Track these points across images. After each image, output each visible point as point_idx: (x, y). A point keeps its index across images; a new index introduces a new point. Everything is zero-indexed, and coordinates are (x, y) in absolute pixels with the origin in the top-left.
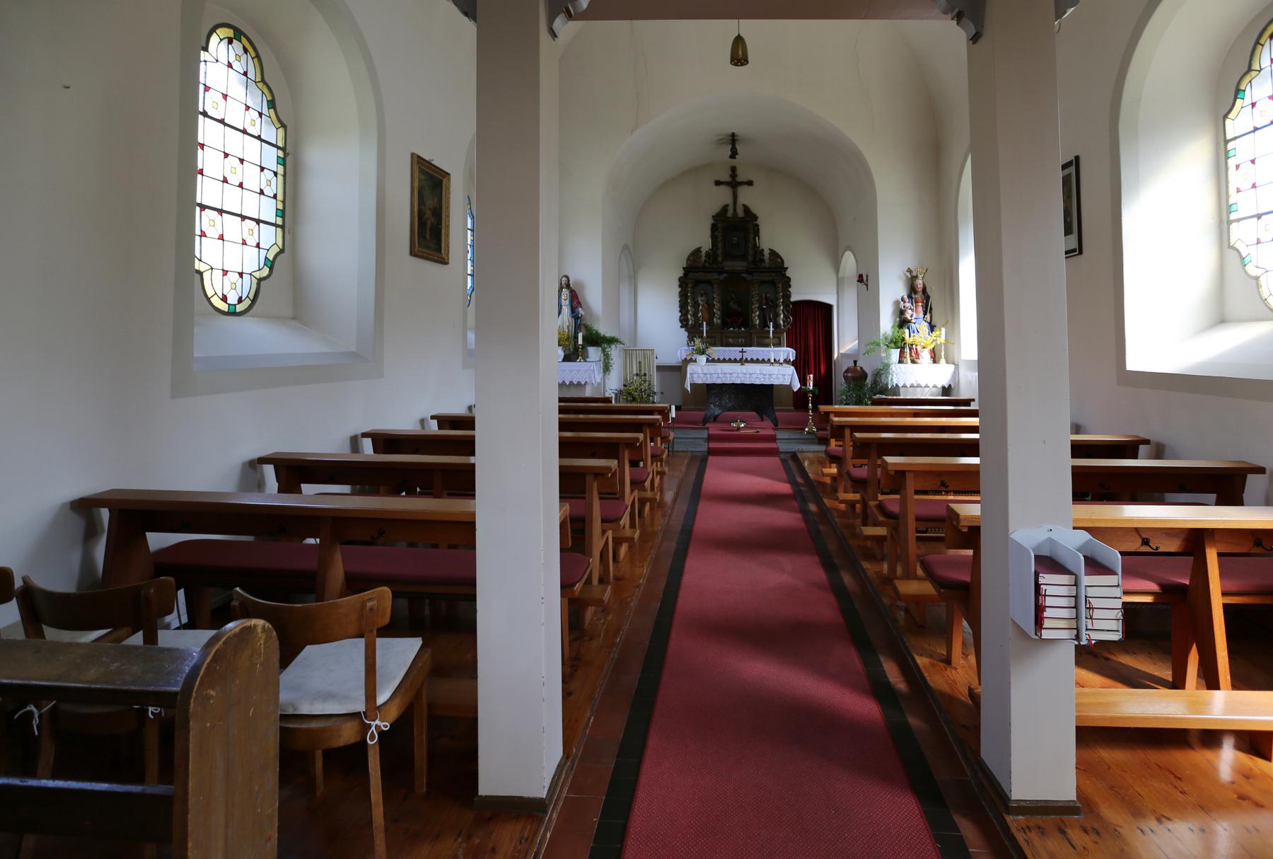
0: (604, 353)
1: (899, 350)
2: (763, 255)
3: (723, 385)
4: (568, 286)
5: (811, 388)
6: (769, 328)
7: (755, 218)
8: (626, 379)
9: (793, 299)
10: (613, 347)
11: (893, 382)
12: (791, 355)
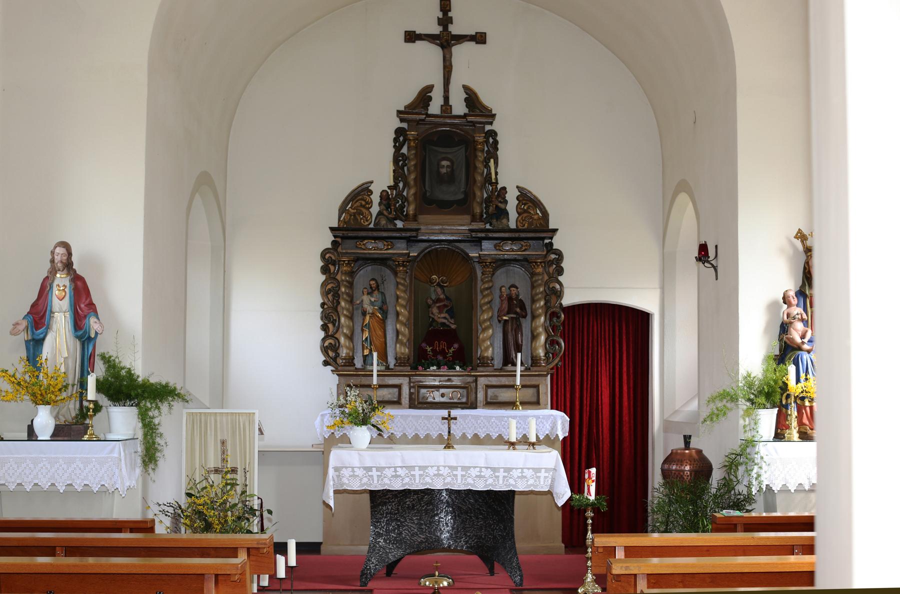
0: (143, 420)
1: (776, 410)
2: (506, 202)
3: (406, 493)
4: (68, 265)
5: (592, 497)
6: (514, 365)
7: (490, 116)
8: (191, 480)
9: (568, 300)
10: (164, 407)
11: (760, 483)
12: (559, 427)
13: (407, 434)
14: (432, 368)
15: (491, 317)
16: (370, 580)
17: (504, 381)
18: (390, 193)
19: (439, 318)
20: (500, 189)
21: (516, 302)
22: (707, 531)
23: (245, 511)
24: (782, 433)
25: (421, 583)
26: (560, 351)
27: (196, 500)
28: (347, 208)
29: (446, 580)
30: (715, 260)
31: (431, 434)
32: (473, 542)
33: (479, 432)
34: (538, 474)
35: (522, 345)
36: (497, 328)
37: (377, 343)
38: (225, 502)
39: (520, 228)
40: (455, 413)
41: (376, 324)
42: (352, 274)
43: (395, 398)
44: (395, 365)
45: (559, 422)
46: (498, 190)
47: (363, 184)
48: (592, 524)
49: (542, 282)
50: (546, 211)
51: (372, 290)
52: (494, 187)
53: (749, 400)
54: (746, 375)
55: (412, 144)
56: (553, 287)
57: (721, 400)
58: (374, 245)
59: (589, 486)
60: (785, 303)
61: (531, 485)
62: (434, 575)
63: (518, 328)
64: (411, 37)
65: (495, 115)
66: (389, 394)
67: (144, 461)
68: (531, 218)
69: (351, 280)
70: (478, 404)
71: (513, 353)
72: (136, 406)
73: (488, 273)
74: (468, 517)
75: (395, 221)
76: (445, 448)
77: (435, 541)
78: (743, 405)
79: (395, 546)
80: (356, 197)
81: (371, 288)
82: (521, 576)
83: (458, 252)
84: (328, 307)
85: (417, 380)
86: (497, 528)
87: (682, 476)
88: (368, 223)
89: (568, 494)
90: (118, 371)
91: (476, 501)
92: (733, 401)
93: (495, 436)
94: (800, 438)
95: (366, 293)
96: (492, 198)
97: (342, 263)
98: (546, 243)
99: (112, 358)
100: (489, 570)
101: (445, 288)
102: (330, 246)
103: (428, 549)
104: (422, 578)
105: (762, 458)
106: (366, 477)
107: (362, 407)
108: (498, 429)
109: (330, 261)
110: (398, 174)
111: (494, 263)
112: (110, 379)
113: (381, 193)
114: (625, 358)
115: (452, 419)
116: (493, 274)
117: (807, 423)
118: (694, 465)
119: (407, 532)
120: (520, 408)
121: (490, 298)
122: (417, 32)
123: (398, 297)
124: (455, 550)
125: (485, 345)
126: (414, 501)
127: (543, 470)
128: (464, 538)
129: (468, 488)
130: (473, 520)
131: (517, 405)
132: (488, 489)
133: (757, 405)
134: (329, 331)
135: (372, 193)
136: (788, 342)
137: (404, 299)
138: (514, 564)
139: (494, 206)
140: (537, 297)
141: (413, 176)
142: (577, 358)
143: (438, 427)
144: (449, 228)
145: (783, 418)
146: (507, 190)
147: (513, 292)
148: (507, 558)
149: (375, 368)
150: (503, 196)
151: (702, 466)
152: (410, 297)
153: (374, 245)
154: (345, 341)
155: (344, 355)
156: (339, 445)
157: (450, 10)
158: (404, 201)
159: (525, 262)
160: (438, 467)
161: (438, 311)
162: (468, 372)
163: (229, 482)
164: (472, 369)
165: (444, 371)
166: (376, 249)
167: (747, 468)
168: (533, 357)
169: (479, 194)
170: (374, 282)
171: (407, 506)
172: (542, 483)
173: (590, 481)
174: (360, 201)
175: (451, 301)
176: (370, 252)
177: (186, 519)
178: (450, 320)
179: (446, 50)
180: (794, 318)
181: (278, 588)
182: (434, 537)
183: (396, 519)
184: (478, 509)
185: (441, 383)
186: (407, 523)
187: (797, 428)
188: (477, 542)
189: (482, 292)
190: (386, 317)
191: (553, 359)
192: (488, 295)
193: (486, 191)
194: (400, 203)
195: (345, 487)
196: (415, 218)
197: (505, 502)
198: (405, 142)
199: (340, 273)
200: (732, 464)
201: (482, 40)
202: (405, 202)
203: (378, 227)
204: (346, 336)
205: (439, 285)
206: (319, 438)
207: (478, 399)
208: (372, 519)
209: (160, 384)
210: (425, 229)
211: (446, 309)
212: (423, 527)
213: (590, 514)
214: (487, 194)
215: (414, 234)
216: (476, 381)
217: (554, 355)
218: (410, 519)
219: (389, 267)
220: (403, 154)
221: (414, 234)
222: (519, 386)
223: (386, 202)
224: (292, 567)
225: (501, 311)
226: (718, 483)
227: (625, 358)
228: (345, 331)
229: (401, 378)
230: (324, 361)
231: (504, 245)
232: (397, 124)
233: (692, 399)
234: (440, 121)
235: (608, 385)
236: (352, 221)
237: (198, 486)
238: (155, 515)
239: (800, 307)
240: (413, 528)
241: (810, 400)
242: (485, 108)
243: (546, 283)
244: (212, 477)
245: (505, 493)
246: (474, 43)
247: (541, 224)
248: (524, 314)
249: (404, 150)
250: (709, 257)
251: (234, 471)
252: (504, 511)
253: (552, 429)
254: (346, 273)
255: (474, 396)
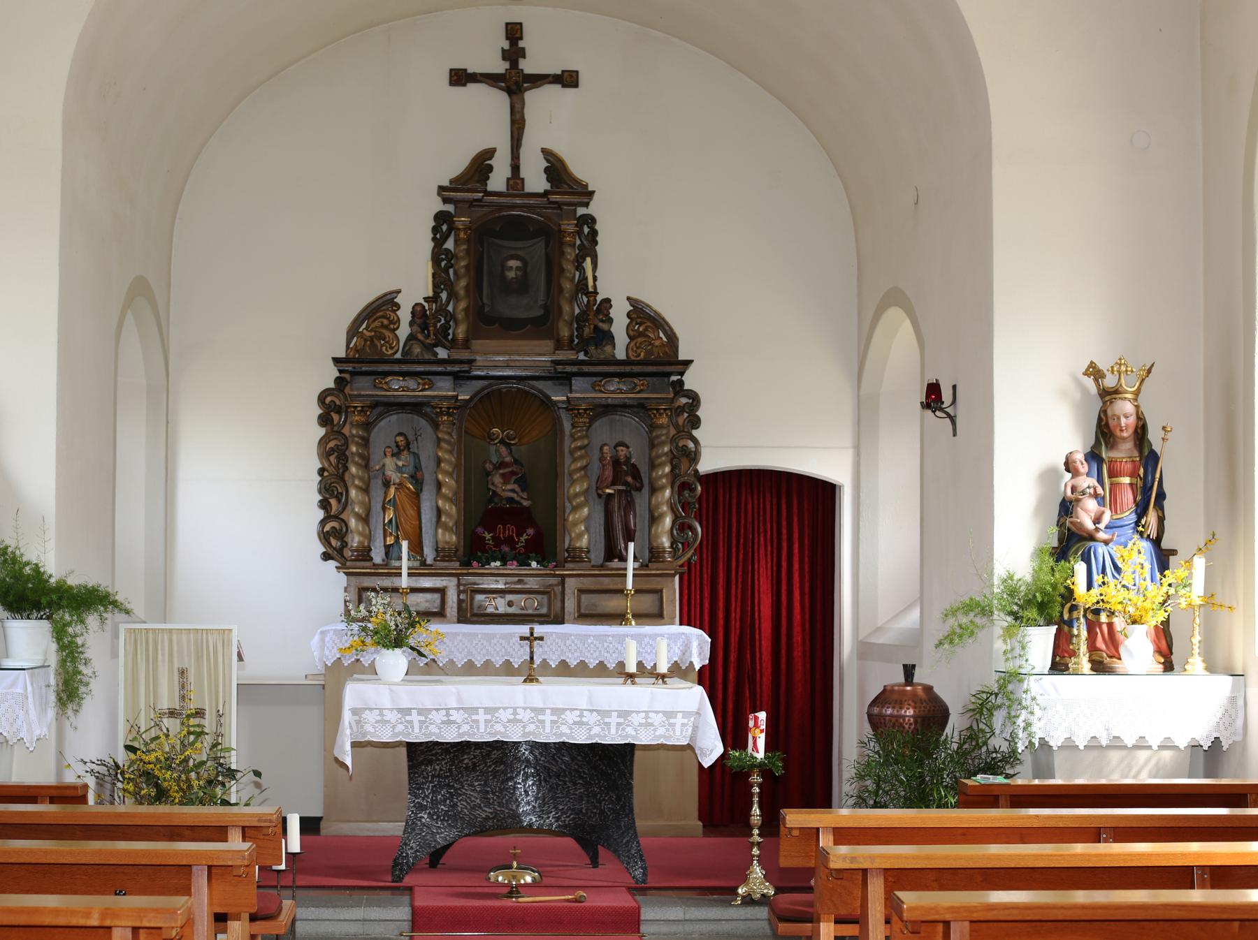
5: (760, 755)
6: (623, 559)
7: (587, 195)
8: (133, 727)
9: (708, 463)
10: (92, 620)
13: (455, 660)
14: (493, 564)
15: (587, 491)
16: (406, 873)
17: (607, 583)
18: (427, 308)
19: (504, 490)
20: (601, 302)
21: (627, 467)
22: (946, 806)
23: (220, 772)
24: (1062, 662)
25: (490, 878)
26: (695, 540)
27: (144, 757)
28: (361, 330)
29: (530, 874)
30: (953, 406)
31: (493, 660)
32: (568, 819)
33: (568, 657)
34: (672, 721)
35: (635, 531)
36: (596, 506)
37: (408, 528)
38: (186, 760)
39: (633, 358)
40: (539, 629)
41: (405, 499)
42: (368, 426)
43: (436, 608)
44: (435, 560)
45: (695, 644)
46: (598, 302)
47: (385, 295)
48: (760, 795)
49: (667, 438)
50: (674, 334)
51: (399, 449)
52: (591, 299)
53: (1011, 613)
54: (1005, 578)
55: (462, 235)
56: (684, 446)
57: (966, 614)
58: (402, 383)
59: (755, 739)
60: (1068, 470)
61: (661, 736)
62: (510, 867)
63: (629, 506)
64: (460, 78)
65: (593, 192)
66: (427, 601)
67: (60, 699)
68: (650, 344)
69: (366, 435)
70: (566, 617)
71: (622, 541)
72: (48, 618)
73: (581, 425)
74: (560, 783)
75: (435, 349)
76: (525, 681)
77: (509, 816)
78: (1002, 621)
79: (446, 824)
80: (374, 314)
81: (398, 446)
82: (644, 869)
83: (534, 394)
84: (330, 475)
85: (469, 581)
86: (606, 798)
87: (901, 724)
88: (392, 352)
89: (719, 749)
90: (20, 568)
91: (573, 759)
92: (985, 615)
93: (592, 663)
94: (1092, 669)
95: (390, 454)
96: (588, 315)
97: (353, 409)
98: (673, 381)
99: (10, 550)
100: (591, 859)
101: (512, 447)
102: (332, 385)
103: (497, 829)
104: (491, 871)
105: (1034, 699)
106: (401, 723)
107: (395, 621)
108: (597, 653)
109: (333, 407)
110: (440, 280)
111: (591, 410)
112: (7, 579)
113: (413, 308)
114: (796, 551)
115: (536, 639)
116: (590, 426)
117: (1103, 647)
118: (920, 707)
119: (464, 803)
120: (633, 623)
121: (584, 462)
122: (470, 71)
123: (439, 461)
124: (540, 831)
125: (577, 531)
126: (475, 757)
127: (680, 715)
128: (554, 813)
129: (561, 741)
130: (569, 787)
131: (628, 619)
132: (594, 741)
133: (1025, 620)
134: (331, 510)
135: (399, 307)
136: (1073, 529)
137: (449, 462)
138: (633, 852)
139: (592, 327)
140: (660, 460)
141: (463, 283)
142: (721, 550)
143: (503, 650)
144: (521, 359)
145: (1064, 640)
146: (612, 303)
147: (621, 453)
148: (622, 842)
149: (405, 563)
150: (605, 312)
151: (934, 710)
152: (458, 459)
153: (402, 383)
154: (357, 525)
155: (355, 545)
156: (355, 676)
157: (521, 38)
158: (448, 319)
159: (641, 408)
160: (515, 709)
161: (502, 481)
162: (551, 570)
163: (192, 729)
164: (556, 566)
165: (513, 567)
166: (405, 389)
167: (1009, 713)
168: (652, 548)
169: (568, 309)
170: (402, 438)
171: (464, 766)
172: (678, 733)
173: (757, 731)
174: (380, 320)
175: (522, 466)
176: (396, 393)
177: (128, 783)
178: (521, 494)
179: (515, 97)
180: (1083, 493)
181: (276, 884)
182: (507, 811)
183: (448, 785)
184: (577, 771)
185: (507, 586)
186: (464, 791)
187: (1087, 655)
188: (574, 818)
189: (572, 452)
190: (421, 490)
191: (683, 551)
192: (581, 457)
193: (578, 305)
194: (443, 321)
195: (369, 738)
196: (466, 344)
197: (619, 761)
198: (451, 233)
199: (347, 426)
200: (982, 707)
201: (572, 82)
202: (449, 321)
203: (409, 357)
204: (358, 516)
205: (502, 442)
206: (317, 666)
207: (566, 610)
208: (410, 784)
209: (85, 587)
210: (483, 360)
211: (514, 478)
212: (490, 796)
213: (756, 779)
214: (579, 307)
215: (465, 367)
216: (563, 583)
217: (686, 545)
218: (469, 785)
219: (425, 416)
220: (447, 250)
221: (465, 367)
222: (630, 590)
223: (421, 320)
224: (294, 854)
225: (602, 481)
226: (960, 736)
227: (796, 551)
228: (357, 510)
229: (443, 578)
230: (324, 554)
231: (608, 384)
232: (438, 205)
233: (909, 607)
234: (505, 201)
235: (770, 589)
236: (367, 348)
237: (144, 736)
238: (79, 777)
239: (1092, 477)
240: (475, 797)
241: (1108, 614)
242: (577, 182)
243: (673, 440)
244: (167, 722)
245: (620, 748)
246: (560, 86)
247: (665, 353)
248: (638, 485)
249: (450, 244)
250: (943, 403)
251: (200, 713)
252: (617, 774)
253: (684, 654)
254: (359, 425)
255: (559, 604)
